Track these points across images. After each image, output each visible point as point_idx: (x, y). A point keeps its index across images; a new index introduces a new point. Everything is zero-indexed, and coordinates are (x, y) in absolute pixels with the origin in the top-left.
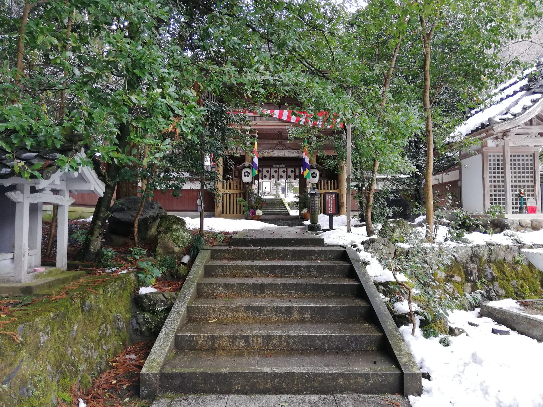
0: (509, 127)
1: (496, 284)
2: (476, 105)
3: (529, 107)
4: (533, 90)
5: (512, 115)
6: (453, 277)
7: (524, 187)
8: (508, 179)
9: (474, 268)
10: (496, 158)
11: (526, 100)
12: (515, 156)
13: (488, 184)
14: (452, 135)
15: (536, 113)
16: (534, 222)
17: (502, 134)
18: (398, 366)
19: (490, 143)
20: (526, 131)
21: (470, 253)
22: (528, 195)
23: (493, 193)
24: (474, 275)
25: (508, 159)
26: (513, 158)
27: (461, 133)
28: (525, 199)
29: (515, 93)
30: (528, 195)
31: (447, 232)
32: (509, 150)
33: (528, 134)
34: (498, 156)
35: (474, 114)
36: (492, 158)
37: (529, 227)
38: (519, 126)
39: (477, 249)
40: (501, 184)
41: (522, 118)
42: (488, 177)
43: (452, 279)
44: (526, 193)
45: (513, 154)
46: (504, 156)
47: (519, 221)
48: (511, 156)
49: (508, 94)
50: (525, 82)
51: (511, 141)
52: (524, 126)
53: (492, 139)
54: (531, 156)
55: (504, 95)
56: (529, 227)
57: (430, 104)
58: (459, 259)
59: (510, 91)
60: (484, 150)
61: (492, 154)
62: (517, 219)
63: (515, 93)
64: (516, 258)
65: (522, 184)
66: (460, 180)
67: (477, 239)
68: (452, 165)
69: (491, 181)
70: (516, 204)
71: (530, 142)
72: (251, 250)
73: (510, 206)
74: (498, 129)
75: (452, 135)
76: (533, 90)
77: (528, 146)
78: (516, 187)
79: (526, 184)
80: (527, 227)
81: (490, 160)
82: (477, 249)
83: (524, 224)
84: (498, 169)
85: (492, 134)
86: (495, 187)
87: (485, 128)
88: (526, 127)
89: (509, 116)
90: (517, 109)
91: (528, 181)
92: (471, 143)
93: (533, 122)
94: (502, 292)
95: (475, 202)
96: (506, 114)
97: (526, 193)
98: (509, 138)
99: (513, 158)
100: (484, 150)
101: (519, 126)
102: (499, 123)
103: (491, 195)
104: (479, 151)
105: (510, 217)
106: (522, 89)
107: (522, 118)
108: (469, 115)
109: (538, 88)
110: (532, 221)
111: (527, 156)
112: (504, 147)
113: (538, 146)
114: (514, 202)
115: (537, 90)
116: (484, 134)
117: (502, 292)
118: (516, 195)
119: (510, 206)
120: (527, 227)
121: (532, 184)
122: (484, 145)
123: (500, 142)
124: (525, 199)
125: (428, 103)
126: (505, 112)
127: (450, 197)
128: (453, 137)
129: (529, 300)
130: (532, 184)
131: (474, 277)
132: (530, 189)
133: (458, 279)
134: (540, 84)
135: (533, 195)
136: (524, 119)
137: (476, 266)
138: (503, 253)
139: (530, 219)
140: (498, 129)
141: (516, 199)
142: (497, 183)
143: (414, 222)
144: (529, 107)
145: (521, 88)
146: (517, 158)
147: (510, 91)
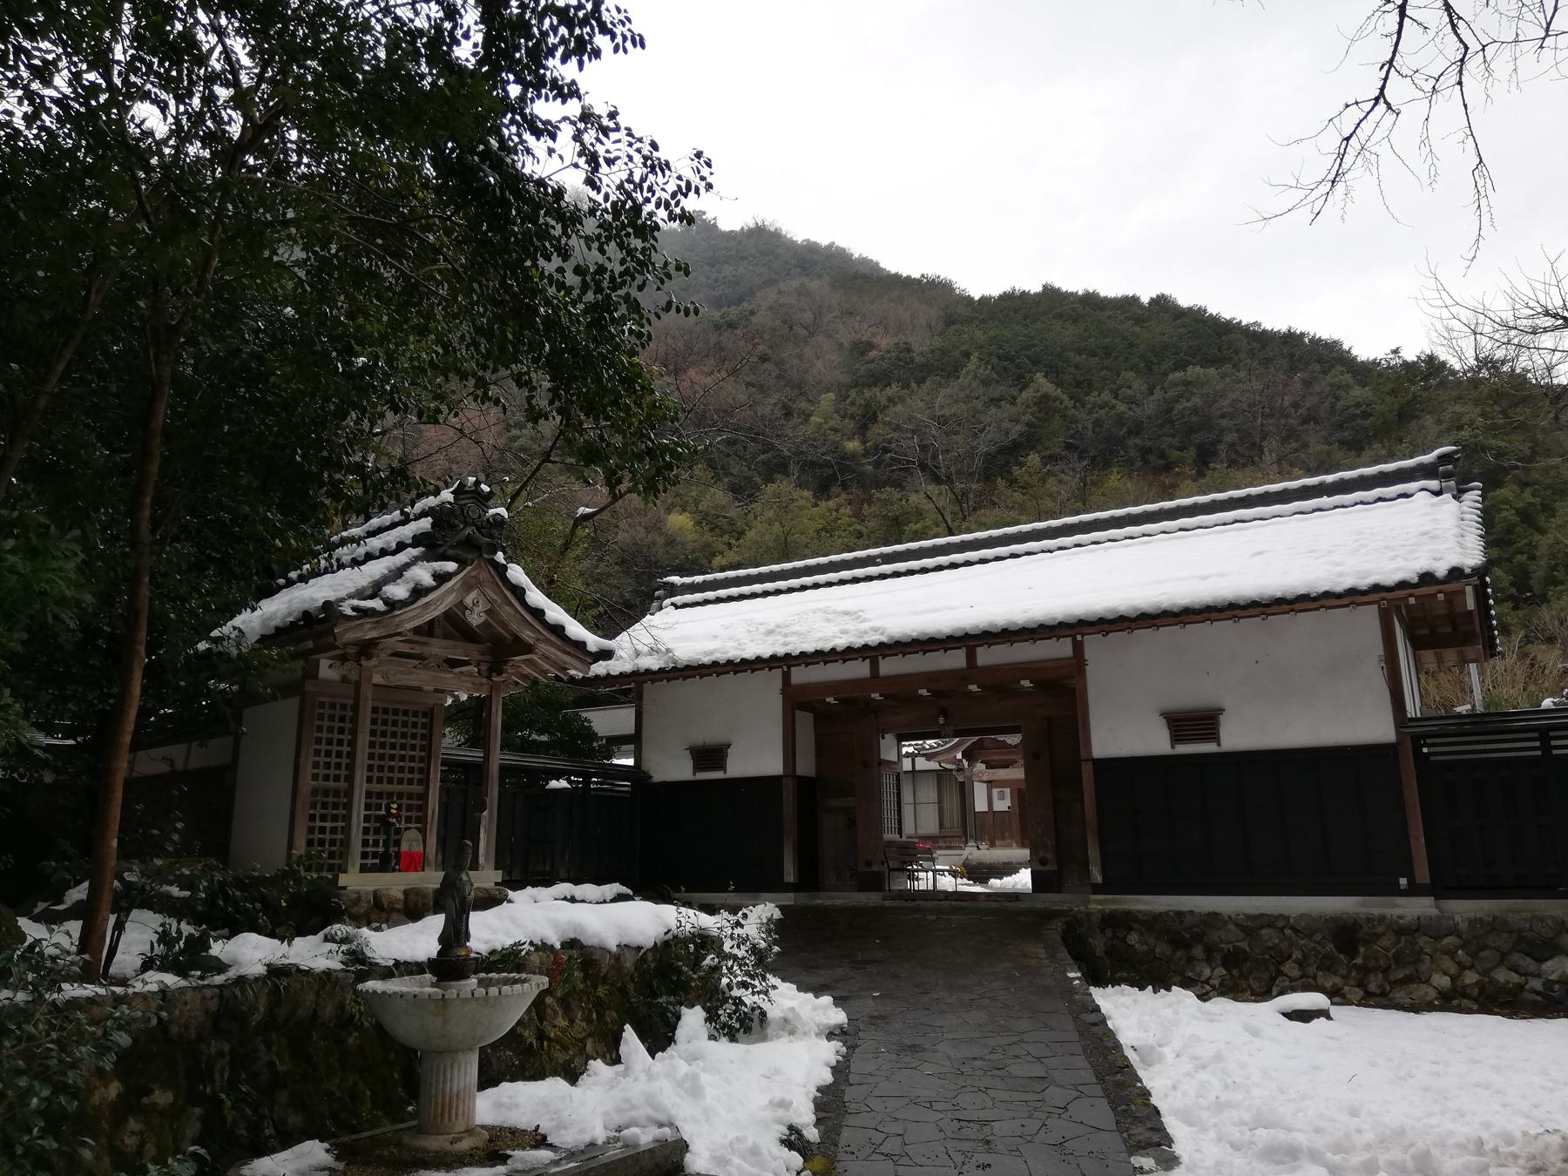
0: (373, 634)
1: (282, 1097)
2: (307, 557)
3: (429, 590)
4: (441, 550)
5: (386, 603)
6: (149, 1092)
7: (400, 796)
8: (360, 776)
9: (221, 1054)
10: (338, 713)
11: (423, 574)
12: (386, 711)
13: (307, 784)
14: (215, 633)
15: (442, 608)
16: (412, 896)
17: (356, 649)
18: (1315, 1157)
19: (327, 670)
20: (417, 650)
21: (213, 1005)
22: (408, 820)
23: (319, 811)
24: (217, 1076)
25: (366, 716)
26: (381, 716)
27: (240, 630)
28: (398, 831)
29: (401, 547)
30: (408, 820)
31: (155, 938)
32: (369, 695)
33: (420, 657)
34: (344, 707)
35: (341, 566)
36: (327, 712)
37: (398, 911)
38: (399, 634)
39: (237, 991)
40: (343, 785)
41: (410, 615)
42: (310, 764)
43: (145, 1100)
44: (404, 813)
45: (381, 705)
46: (355, 708)
47: (375, 892)
48: (375, 710)
49: (403, 539)
50: (426, 524)
51: (379, 673)
52: (410, 636)
53: (331, 658)
54: (425, 715)
55: (375, 543)
56: (398, 911)
57: (153, 532)
58: (174, 1029)
59: (390, 538)
60: (309, 686)
61: (327, 700)
62: (371, 889)
63: (401, 547)
64: (348, 1008)
65: (395, 788)
66: (232, 767)
67: (251, 952)
68: (221, 721)
69: (315, 777)
70: (376, 843)
71: (423, 679)
72: (1078, 513)
73: (357, 848)
74: (348, 635)
75: (215, 633)
76: (441, 550)
77: (420, 689)
78: (380, 795)
79: (404, 788)
80: (393, 910)
81: (321, 717)
82: (237, 991)
83: (385, 902)
84: (340, 742)
85: (333, 647)
86: (326, 793)
87: (316, 626)
88: (416, 638)
89: (376, 604)
90: (399, 591)
91: (410, 782)
92: (267, 666)
93: (437, 630)
94: (294, 1120)
95: (269, 835)
96: (372, 597)
97: (404, 813)
98: (374, 662)
99: (381, 716)
100: (309, 686)
101: (399, 634)
102: (349, 618)
103: (312, 818)
104: (288, 689)
105: (354, 881)
106: (417, 541)
107: (410, 615)
108: (282, 581)
109: (452, 547)
110: (406, 893)
111: (415, 714)
112: (358, 684)
113: (443, 691)
114: (371, 838)
115: (450, 552)
116: (310, 644)
117: (294, 1120)
118: (378, 818)
119: (357, 848)
120: (393, 910)
121: (420, 789)
122: (312, 673)
123: (349, 669)
124: (398, 831)
125: (145, 526)
126: (370, 592)
127: (179, 825)
128: (217, 640)
129: (368, 1134)
130: (420, 789)
131: (218, 1085)
132: (415, 802)
133: (162, 1098)
134: (457, 539)
135: (418, 820)
136: (413, 618)
137: (226, 1047)
138: (311, 997)
139: (402, 888)
140: (348, 635)
141: (377, 831)
142: (331, 784)
143: (62, 902)
144: (429, 590)
145: (414, 537)
146: (391, 717)
147: (390, 538)
